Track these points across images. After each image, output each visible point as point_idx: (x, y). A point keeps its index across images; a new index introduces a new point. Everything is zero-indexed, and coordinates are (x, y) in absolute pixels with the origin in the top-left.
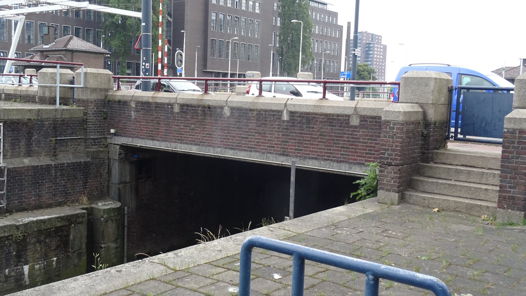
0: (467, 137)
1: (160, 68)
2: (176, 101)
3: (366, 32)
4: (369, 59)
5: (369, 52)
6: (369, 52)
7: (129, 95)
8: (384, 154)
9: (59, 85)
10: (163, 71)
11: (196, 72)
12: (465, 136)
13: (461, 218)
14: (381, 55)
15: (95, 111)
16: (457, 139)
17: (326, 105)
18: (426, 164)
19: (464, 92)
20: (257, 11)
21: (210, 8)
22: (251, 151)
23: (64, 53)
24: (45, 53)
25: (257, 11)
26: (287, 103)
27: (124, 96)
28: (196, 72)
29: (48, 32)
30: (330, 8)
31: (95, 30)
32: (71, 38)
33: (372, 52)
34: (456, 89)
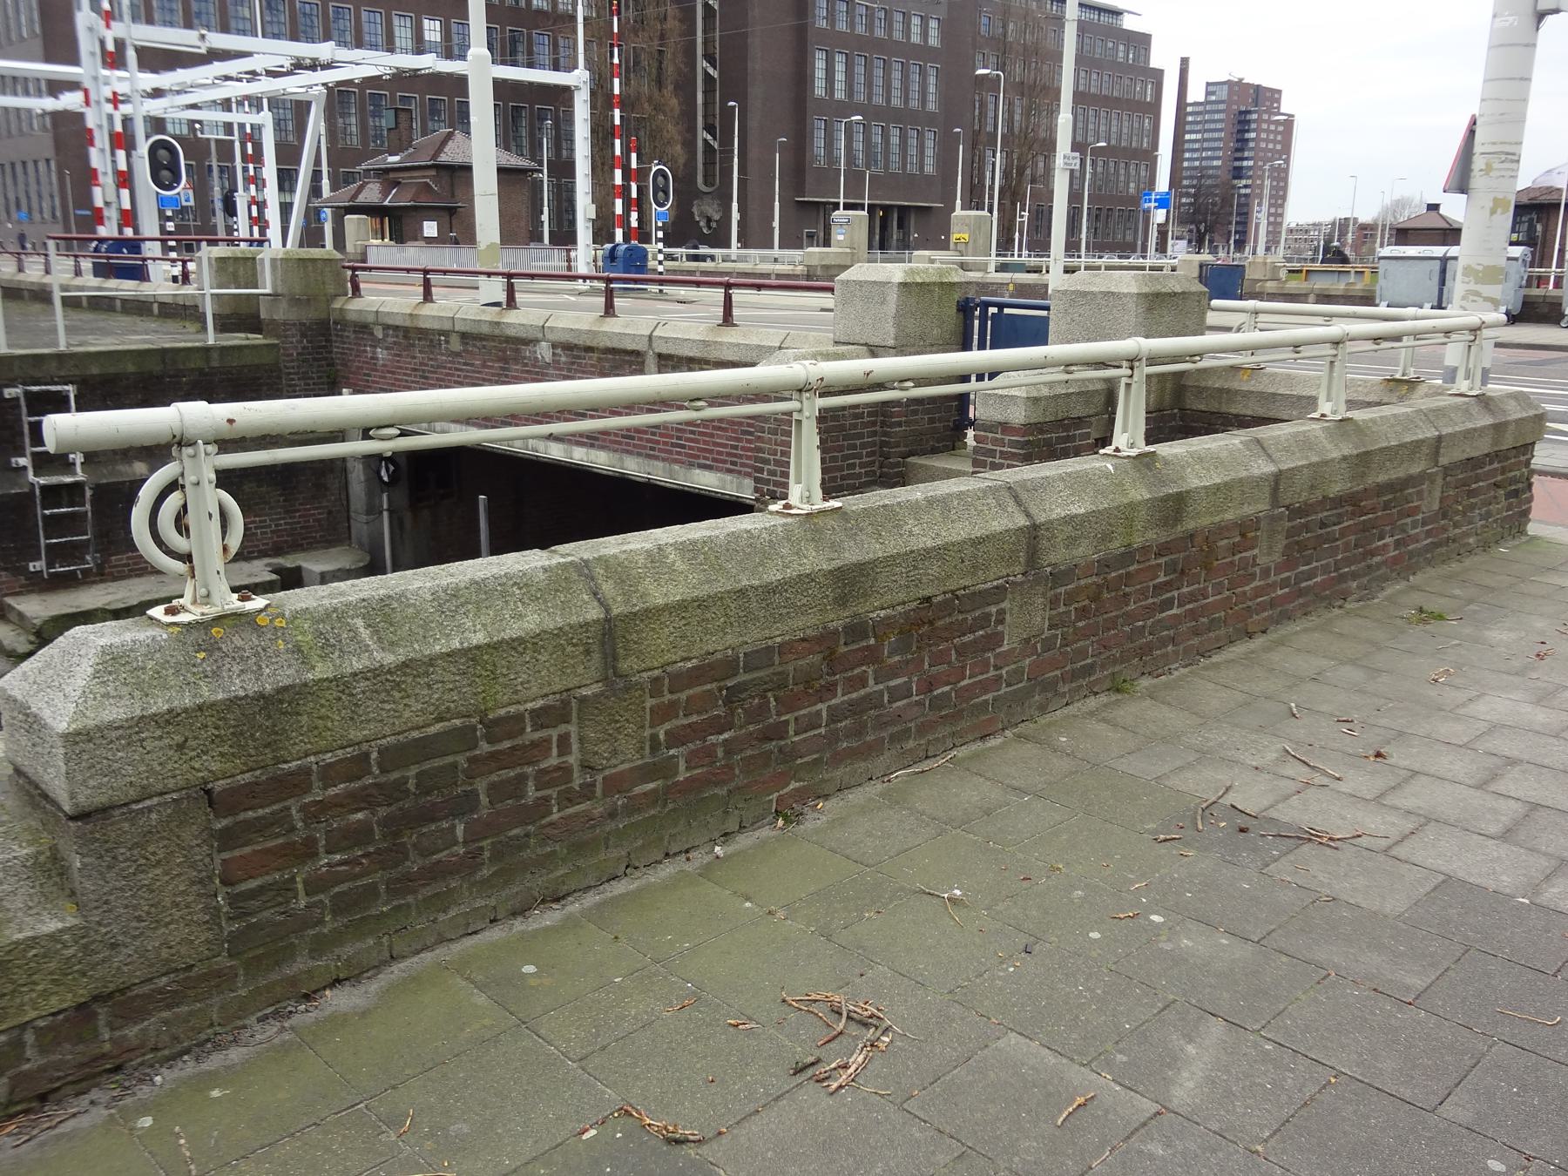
1: (619, 209)
4: (1246, 154)
5: (1247, 136)
6: (1247, 136)
9: (209, 291)
10: (629, 216)
11: (777, 203)
13: (689, 659)
14: (1279, 142)
15: (304, 348)
22: (592, 446)
23: (433, 173)
24: (392, 175)
26: (655, 334)
27: (360, 311)
28: (777, 203)
29: (397, 123)
30: (1128, 23)
31: (531, 107)
32: (449, 136)
33: (1253, 135)
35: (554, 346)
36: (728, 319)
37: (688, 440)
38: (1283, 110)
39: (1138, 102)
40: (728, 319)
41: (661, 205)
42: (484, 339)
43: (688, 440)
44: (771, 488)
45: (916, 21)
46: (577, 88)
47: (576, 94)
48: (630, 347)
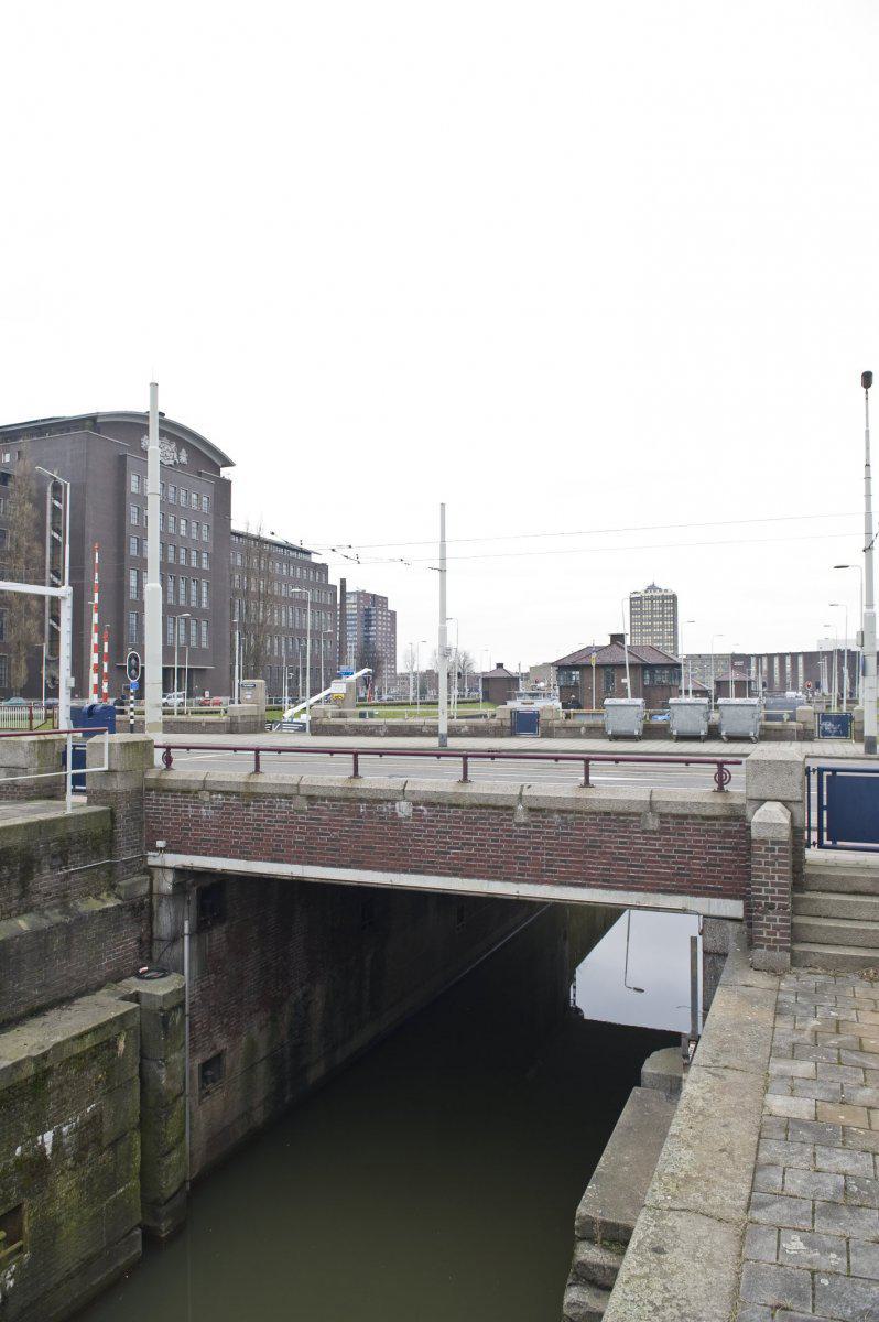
0: (839, 843)
2: (298, 790)
3: (363, 592)
7: (193, 779)
8: (760, 891)
12: (834, 842)
16: (821, 846)
17: (596, 796)
18: (801, 895)
19: (828, 776)
20: (205, 566)
21: (127, 561)
25: (205, 566)
27: (184, 781)
30: (315, 559)
34: (814, 771)
35: (415, 804)
36: (465, 779)
37: (559, 866)
38: (389, 608)
39: (291, 604)
40: (465, 779)
41: (133, 678)
42: (334, 800)
43: (559, 866)
44: (770, 901)
45: (194, 553)
46: (63, 598)
47: (62, 603)
48: (502, 803)
